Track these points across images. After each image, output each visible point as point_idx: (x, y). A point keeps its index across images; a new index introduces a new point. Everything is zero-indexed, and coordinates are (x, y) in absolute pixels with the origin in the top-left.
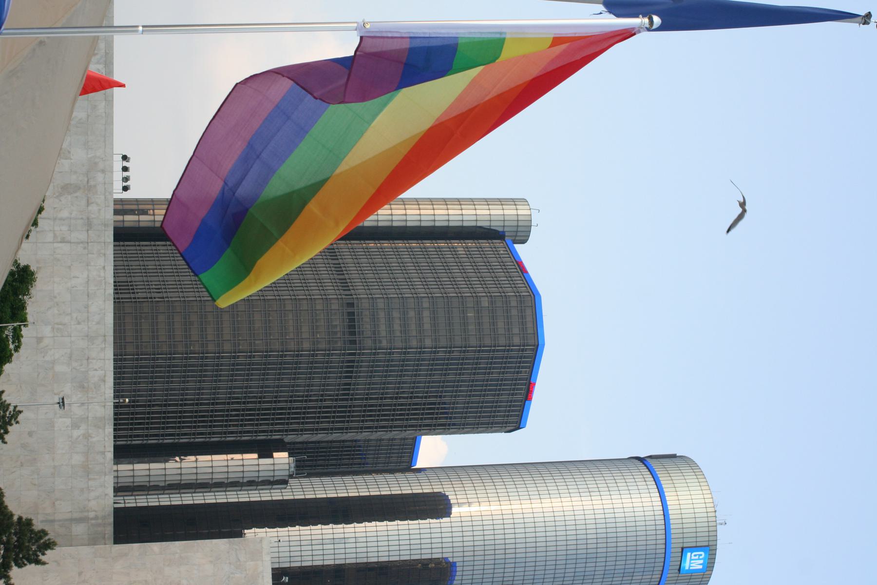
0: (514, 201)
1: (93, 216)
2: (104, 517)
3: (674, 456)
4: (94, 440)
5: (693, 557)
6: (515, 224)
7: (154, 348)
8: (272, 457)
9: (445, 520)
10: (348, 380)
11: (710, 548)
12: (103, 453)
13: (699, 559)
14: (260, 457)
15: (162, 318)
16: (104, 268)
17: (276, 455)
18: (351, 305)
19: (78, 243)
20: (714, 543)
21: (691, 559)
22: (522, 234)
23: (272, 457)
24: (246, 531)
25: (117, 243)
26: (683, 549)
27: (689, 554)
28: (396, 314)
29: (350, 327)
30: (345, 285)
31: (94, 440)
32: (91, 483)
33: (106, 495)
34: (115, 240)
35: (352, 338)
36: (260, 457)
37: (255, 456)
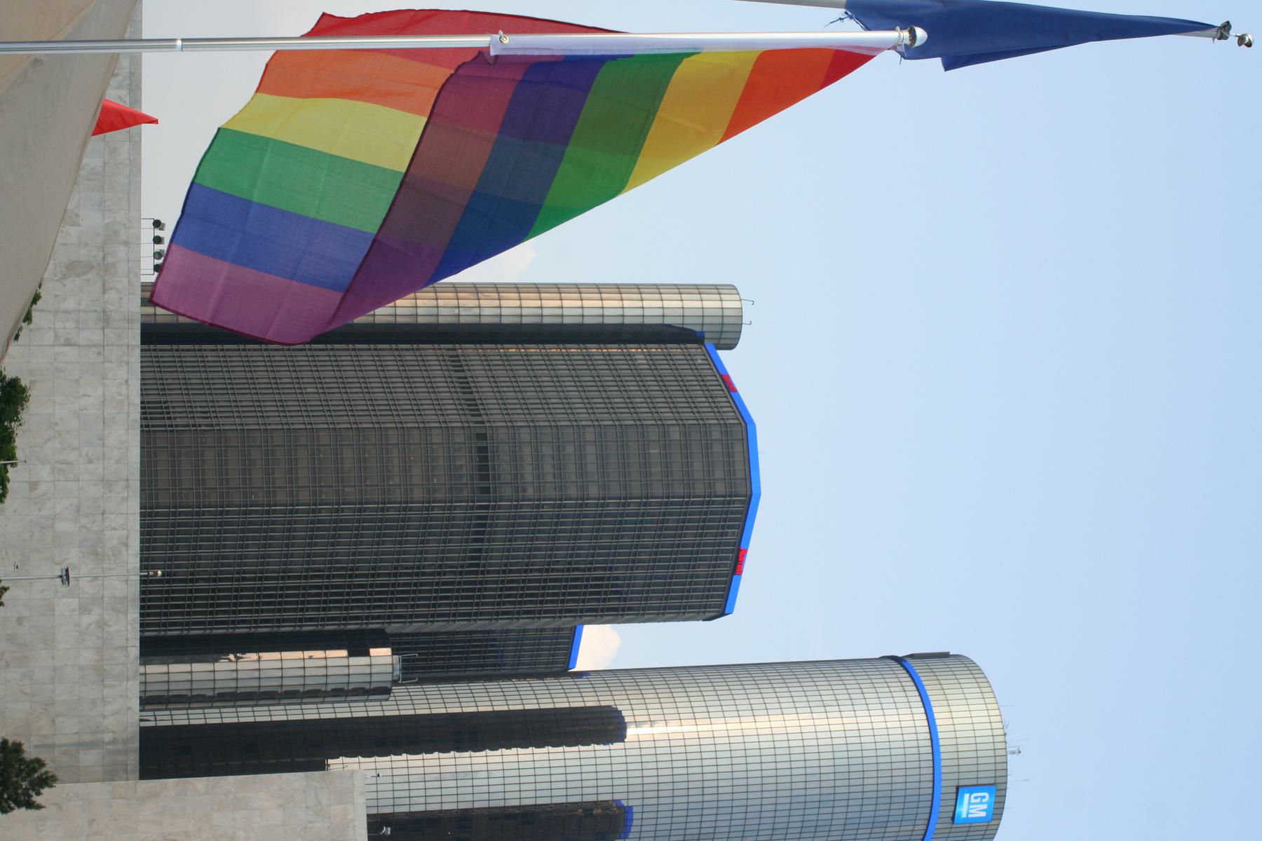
0: (717, 289)
1: (111, 308)
2: (126, 741)
3: (945, 655)
4: (112, 629)
5: (973, 801)
6: (719, 321)
7: (198, 497)
8: (368, 654)
9: (617, 745)
10: (477, 545)
11: (997, 788)
12: (125, 648)
13: (981, 803)
14: (351, 654)
15: (210, 455)
16: (127, 382)
17: (373, 651)
18: (482, 436)
19: (90, 346)
20: (1002, 773)
21: (970, 803)
22: (728, 335)
23: (368, 654)
24: (330, 761)
25: (146, 347)
26: (958, 788)
27: (967, 796)
28: (547, 450)
29: (481, 468)
30: (474, 408)
31: (112, 629)
32: (106, 691)
33: (129, 708)
34: (142, 343)
35: (484, 484)
36: (351, 654)
37: (344, 653)
